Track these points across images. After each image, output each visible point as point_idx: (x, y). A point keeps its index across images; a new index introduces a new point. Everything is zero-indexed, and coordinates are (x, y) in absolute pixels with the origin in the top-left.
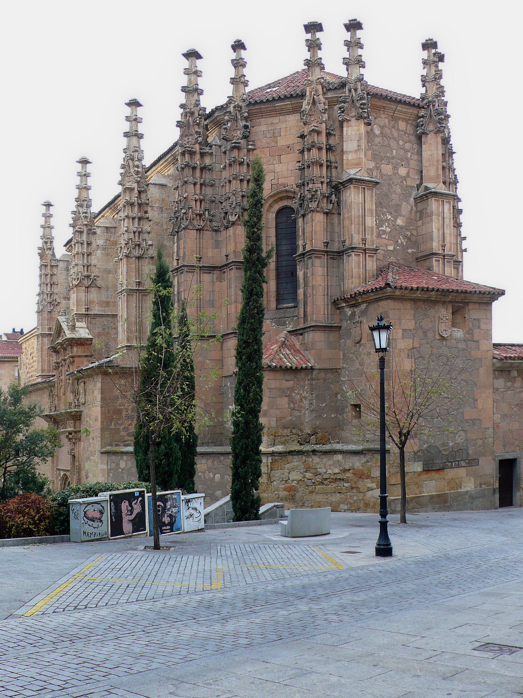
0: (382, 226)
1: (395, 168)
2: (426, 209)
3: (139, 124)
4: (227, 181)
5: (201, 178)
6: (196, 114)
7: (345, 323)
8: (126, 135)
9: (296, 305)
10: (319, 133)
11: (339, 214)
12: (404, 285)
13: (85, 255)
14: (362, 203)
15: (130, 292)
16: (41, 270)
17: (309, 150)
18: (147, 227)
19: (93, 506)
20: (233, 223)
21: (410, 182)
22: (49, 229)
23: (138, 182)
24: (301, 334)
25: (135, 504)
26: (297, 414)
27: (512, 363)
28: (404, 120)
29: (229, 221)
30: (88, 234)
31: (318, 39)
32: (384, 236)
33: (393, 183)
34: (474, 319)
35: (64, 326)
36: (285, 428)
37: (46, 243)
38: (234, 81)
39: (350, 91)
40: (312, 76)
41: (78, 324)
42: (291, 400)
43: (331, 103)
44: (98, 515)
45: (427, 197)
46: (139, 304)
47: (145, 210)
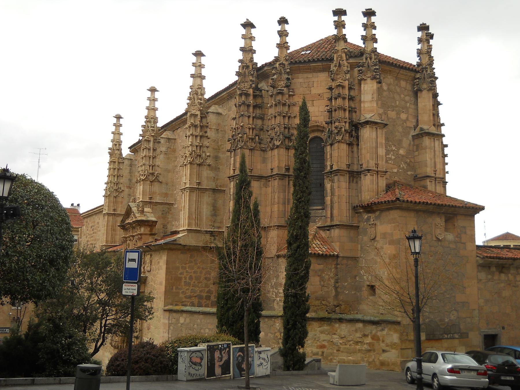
0: (389, 155)
1: (398, 114)
2: (422, 144)
3: (202, 69)
4: (273, 116)
5: (253, 113)
6: (251, 67)
7: (363, 224)
8: (192, 76)
9: (323, 208)
10: (343, 87)
11: (358, 145)
12: (409, 199)
13: (151, 159)
14: (375, 138)
15: (192, 190)
16: (110, 165)
17: (336, 99)
18: (206, 143)
19: (196, 353)
20: (278, 147)
21: (409, 124)
22: (119, 135)
23: (200, 110)
24: (328, 230)
25: (224, 353)
26: (326, 289)
27: (491, 261)
28: (406, 80)
29: (274, 145)
30: (154, 142)
31: (343, 21)
32: (390, 162)
33: (397, 124)
34: (461, 227)
35: (134, 209)
36: (317, 300)
37: (116, 145)
38: (279, 46)
39: (366, 59)
40: (338, 46)
41: (146, 210)
42: (322, 279)
43: (352, 66)
44: (198, 360)
45: (422, 135)
46: (198, 199)
47: (205, 130)
